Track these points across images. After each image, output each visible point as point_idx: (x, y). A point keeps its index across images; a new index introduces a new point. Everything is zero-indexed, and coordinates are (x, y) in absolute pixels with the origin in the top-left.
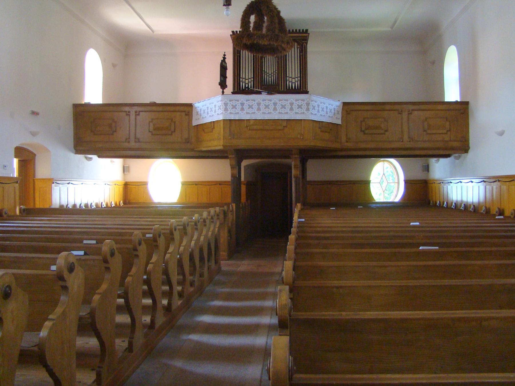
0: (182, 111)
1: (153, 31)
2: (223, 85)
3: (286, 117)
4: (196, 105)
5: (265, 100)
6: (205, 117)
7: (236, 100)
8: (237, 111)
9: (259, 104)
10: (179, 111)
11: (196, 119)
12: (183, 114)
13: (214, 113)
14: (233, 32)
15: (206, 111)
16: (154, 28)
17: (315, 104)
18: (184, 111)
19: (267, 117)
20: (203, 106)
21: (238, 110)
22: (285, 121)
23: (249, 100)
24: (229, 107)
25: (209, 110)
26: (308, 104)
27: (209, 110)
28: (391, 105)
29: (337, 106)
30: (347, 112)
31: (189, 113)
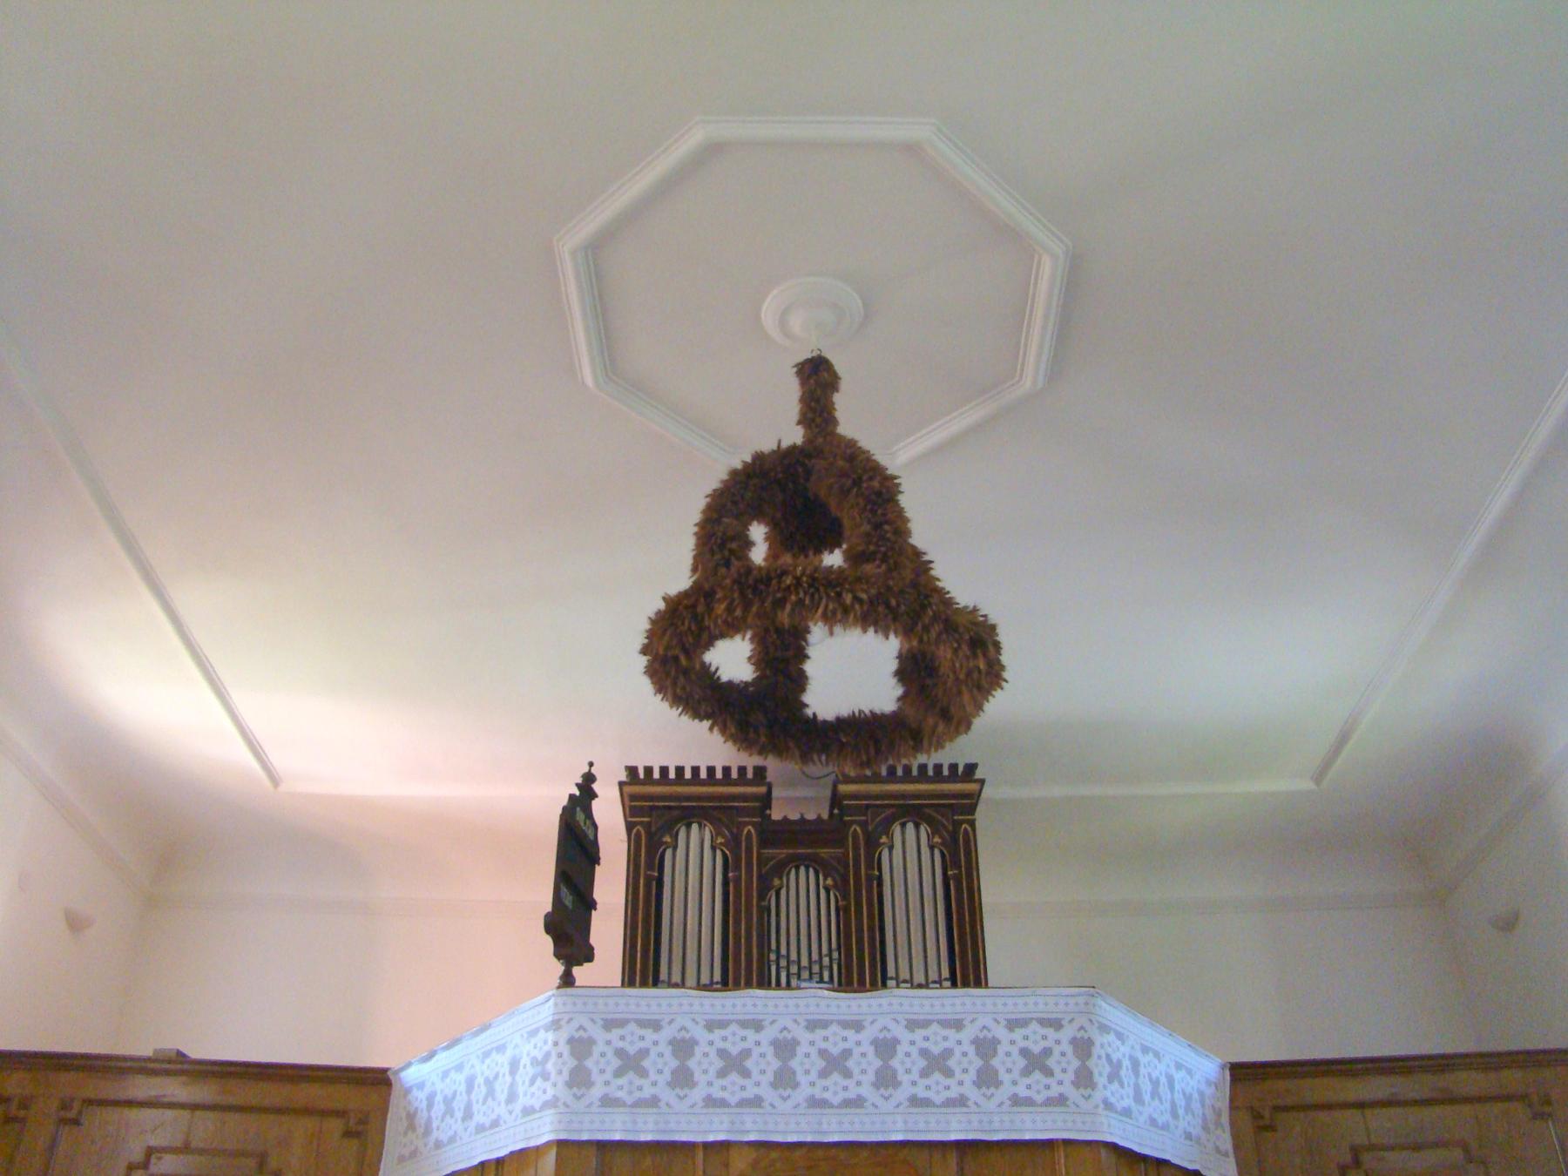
0: (325, 1113)
1: (275, 780)
2: (569, 933)
3: (955, 1129)
4: (411, 1075)
5: (825, 1024)
6: (452, 1140)
7: (642, 1024)
8: (647, 1092)
9: (785, 1048)
10: (308, 1111)
11: (402, 1159)
12: (335, 1126)
13: (502, 1110)
14: (632, 771)
15: (459, 1105)
16: (277, 759)
17: (1121, 1051)
18: (341, 1114)
19: (834, 1129)
20: (445, 1074)
21: (656, 1083)
22: (953, 1158)
23: (723, 1024)
24: (601, 1063)
25: (480, 1091)
26: (1083, 1047)
27: (480, 1091)
28: (1487, 1068)
29: (1208, 1083)
30: (1257, 1116)
31: (363, 1121)
